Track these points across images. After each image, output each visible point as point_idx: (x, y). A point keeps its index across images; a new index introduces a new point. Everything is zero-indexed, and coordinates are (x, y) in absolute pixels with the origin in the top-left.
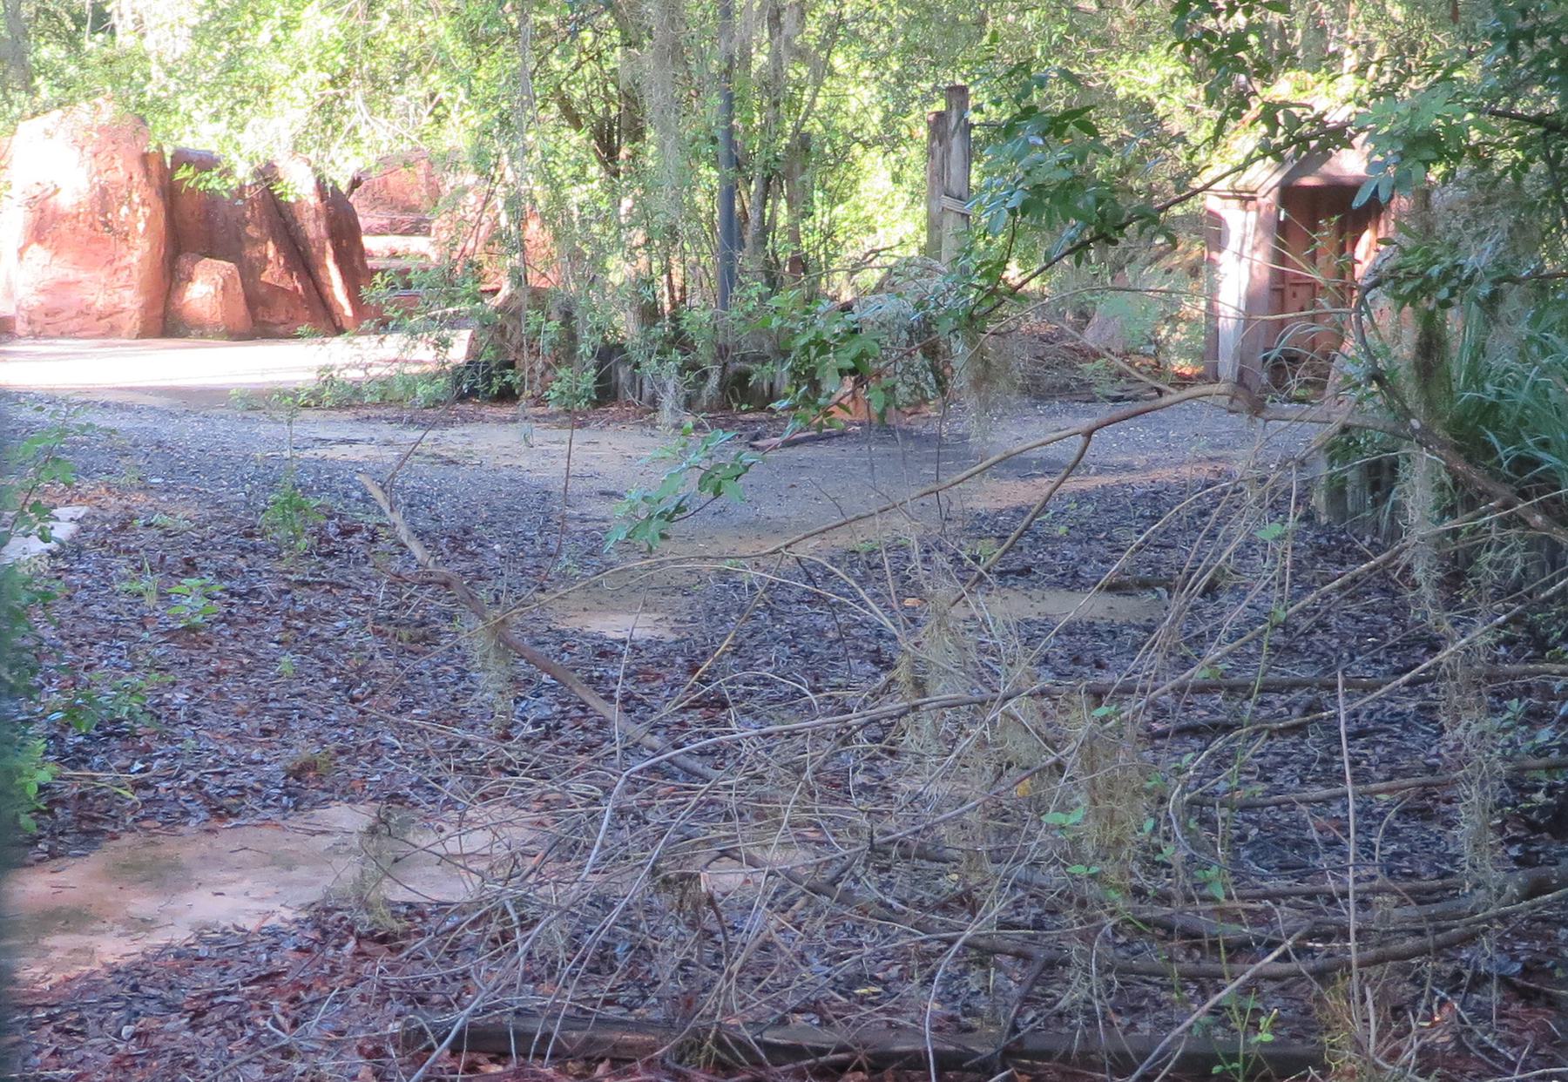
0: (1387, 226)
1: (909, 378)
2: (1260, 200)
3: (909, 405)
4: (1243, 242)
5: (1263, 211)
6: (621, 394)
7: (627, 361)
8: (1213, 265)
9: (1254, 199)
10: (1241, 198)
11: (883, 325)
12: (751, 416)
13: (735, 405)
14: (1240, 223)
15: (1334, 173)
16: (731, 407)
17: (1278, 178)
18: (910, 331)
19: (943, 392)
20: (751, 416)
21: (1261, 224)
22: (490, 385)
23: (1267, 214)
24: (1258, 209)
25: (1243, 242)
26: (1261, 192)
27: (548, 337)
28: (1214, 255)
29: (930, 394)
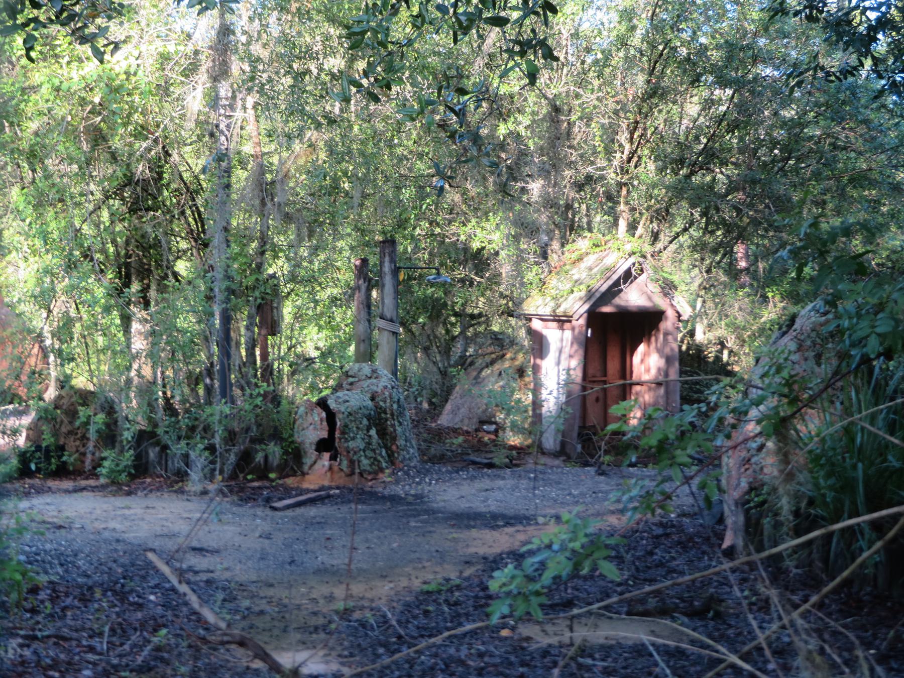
0: (656, 340)
1: (369, 453)
2: (574, 322)
3: (370, 473)
4: (560, 352)
5: (577, 331)
6: (151, 469)
7: (158, 443)
8: (536, 369)
9: (570, 321)
10: (559, 321)
11: (350, 414)
12: (256, 484)
13: (241, 476)
14: (559, 339)
15: (623, 303)
16: (237, 477)
17: (586, 307)
18: (369, 417)
19: (393, 463)
20: (256, 484)
21: (575, 339)
22: (50, 464)
23: (580, 333)
24: (573, 329)
25: (560, 352)
26: (576, 317)
27: (96, 427)
28: (538, 361)
29: (384, 465)
